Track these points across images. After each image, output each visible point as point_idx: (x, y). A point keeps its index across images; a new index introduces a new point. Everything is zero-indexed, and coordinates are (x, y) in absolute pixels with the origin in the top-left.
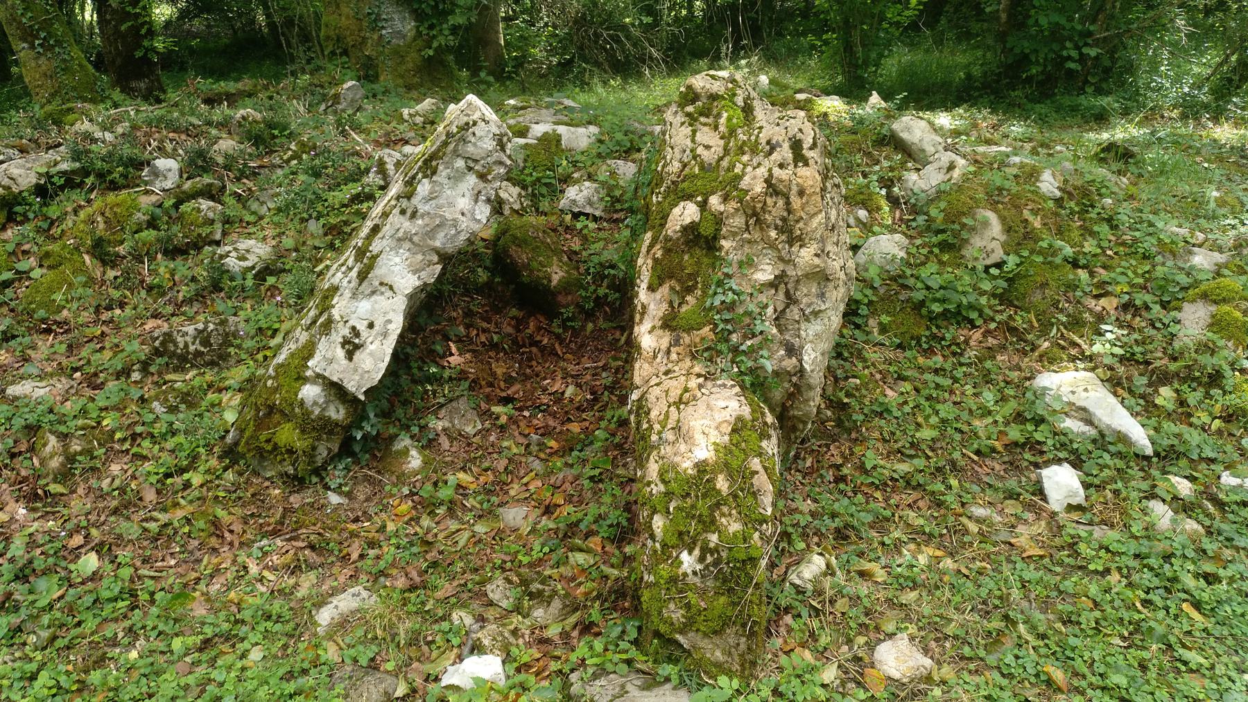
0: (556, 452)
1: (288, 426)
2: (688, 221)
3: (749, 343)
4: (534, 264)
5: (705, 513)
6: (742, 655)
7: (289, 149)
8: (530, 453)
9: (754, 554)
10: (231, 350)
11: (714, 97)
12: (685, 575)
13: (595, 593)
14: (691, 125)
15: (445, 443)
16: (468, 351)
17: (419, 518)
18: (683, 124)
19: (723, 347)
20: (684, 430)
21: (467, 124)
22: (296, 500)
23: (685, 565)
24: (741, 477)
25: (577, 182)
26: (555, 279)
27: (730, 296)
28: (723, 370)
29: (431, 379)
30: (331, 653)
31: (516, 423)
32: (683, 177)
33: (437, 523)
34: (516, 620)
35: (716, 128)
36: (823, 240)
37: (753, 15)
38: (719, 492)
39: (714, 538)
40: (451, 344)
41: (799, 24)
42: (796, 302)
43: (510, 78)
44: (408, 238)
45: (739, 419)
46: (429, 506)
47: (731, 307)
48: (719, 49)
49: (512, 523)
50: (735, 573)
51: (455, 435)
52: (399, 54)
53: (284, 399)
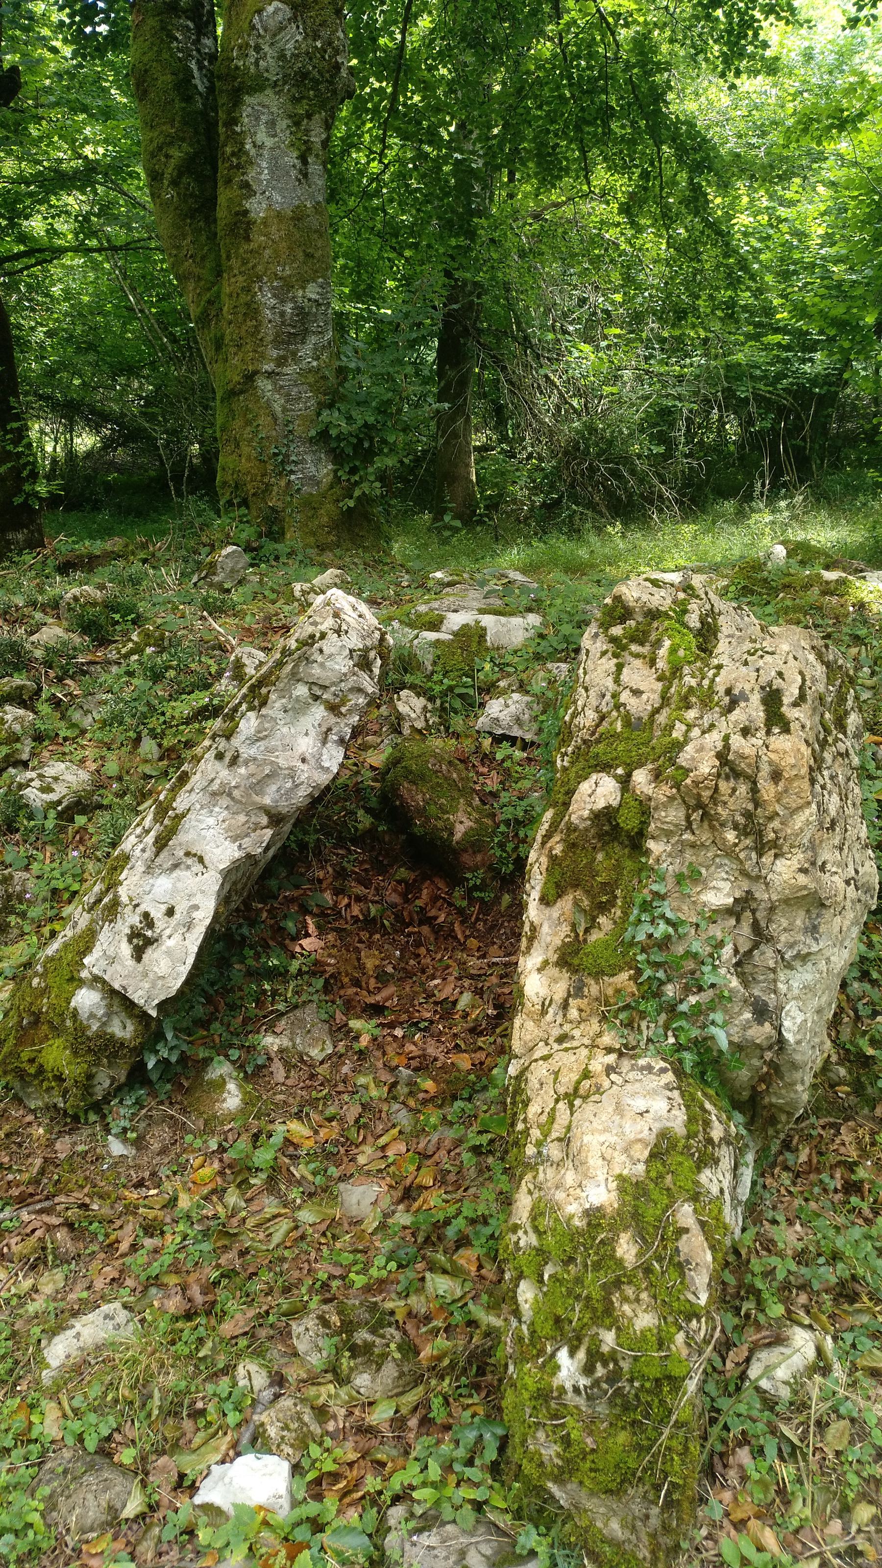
0: (432, 1099)
1: (58, 1042)
2: (601, 804)
3: (693, 1000)
4: (432, 809)
5: (596, 1294)
6: (653, 1536)
7: (130, 640)
8: (395, 1098)
9: (677, 1372)
10: (12, 919)
11: (654, 615)
12: (562, 1390)
13: (446, 1362)
14: (616, 656)
15: (279, 1071)
16: (332, 929)
17: (224, 1190)
18: (604, 653)
19: (650, 1006)
20: (575, 1146)
21: (312, 636)
22: (63, 1147)
23: (563, 1374)
24: (659, 1236)
25: (503, 692)
26: (460, 831)
27: (662, 929)
28: (649, 1040)
29: (273, 974)
30: (49, 1423)
31: (381, 1047)
32: (597, 736)
33: (247, 1201)
34: (325, 1392)
35: (652, 663)
36: (813, 847)
37: (799, 442)
38: (620, 1263)
39: (609, 1339)
40: (309, 920)
41: (863, 452)
42: (769, 940)
43: (481, 522)
44: (225, 792)
45: (664, 1135)
46: (239, 1172)
47: (664, 943)
48: (752, 486)
49: (354, 1211)
50: (645, 1398)
51: (293, 1060)
52: (310, 506)
53: (52, 1007)
